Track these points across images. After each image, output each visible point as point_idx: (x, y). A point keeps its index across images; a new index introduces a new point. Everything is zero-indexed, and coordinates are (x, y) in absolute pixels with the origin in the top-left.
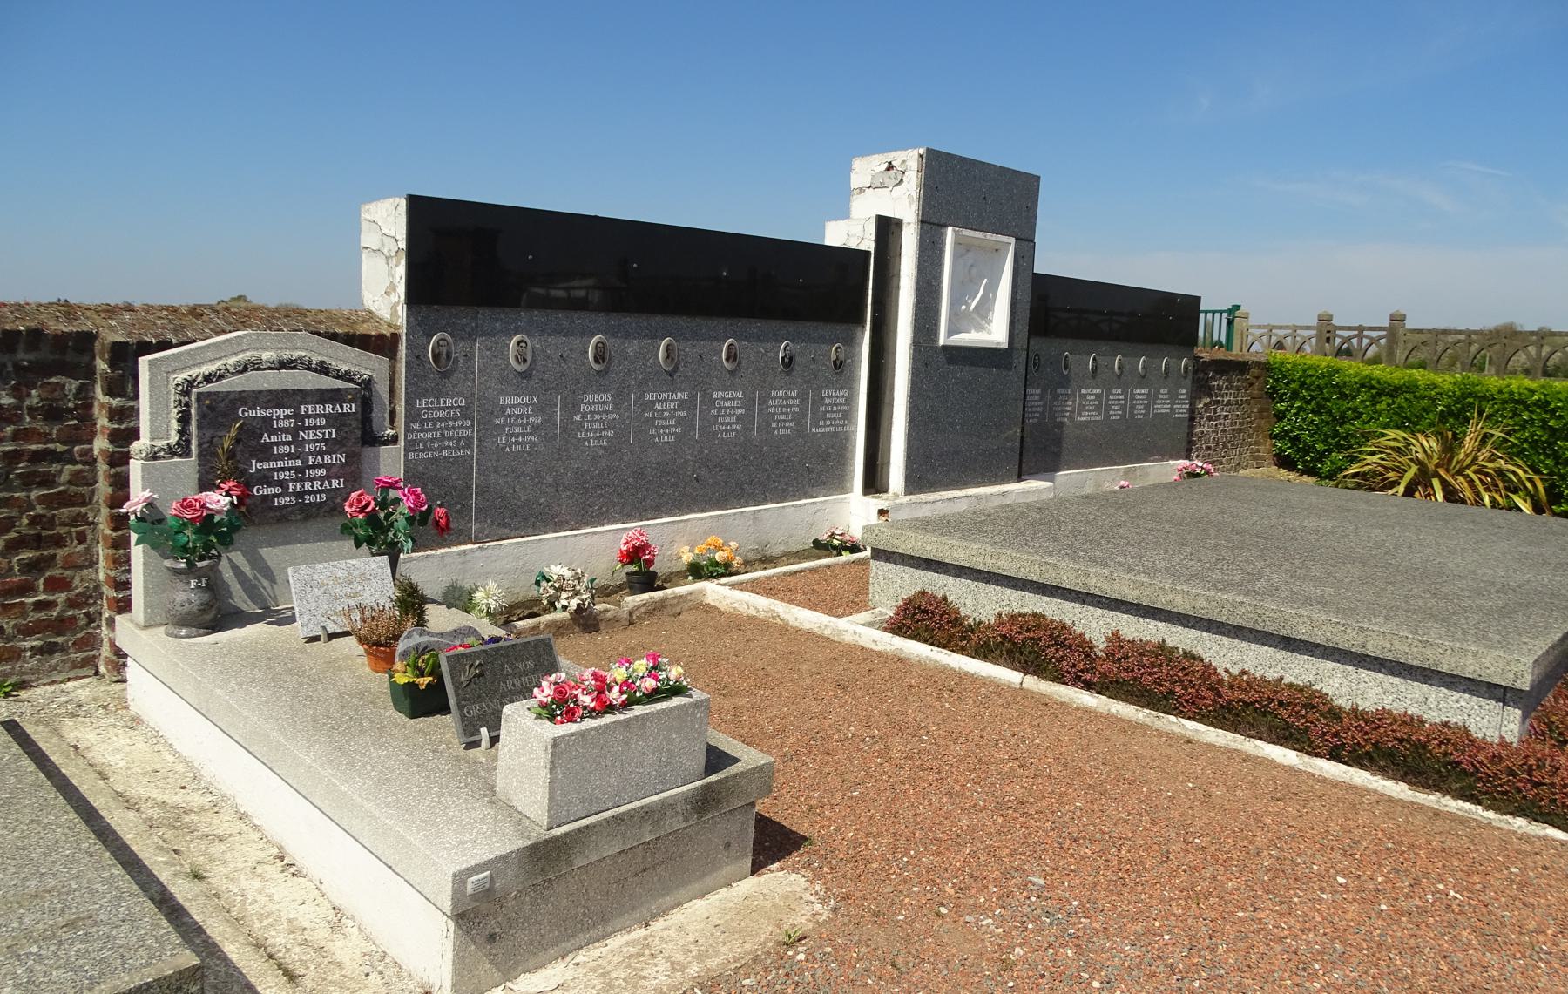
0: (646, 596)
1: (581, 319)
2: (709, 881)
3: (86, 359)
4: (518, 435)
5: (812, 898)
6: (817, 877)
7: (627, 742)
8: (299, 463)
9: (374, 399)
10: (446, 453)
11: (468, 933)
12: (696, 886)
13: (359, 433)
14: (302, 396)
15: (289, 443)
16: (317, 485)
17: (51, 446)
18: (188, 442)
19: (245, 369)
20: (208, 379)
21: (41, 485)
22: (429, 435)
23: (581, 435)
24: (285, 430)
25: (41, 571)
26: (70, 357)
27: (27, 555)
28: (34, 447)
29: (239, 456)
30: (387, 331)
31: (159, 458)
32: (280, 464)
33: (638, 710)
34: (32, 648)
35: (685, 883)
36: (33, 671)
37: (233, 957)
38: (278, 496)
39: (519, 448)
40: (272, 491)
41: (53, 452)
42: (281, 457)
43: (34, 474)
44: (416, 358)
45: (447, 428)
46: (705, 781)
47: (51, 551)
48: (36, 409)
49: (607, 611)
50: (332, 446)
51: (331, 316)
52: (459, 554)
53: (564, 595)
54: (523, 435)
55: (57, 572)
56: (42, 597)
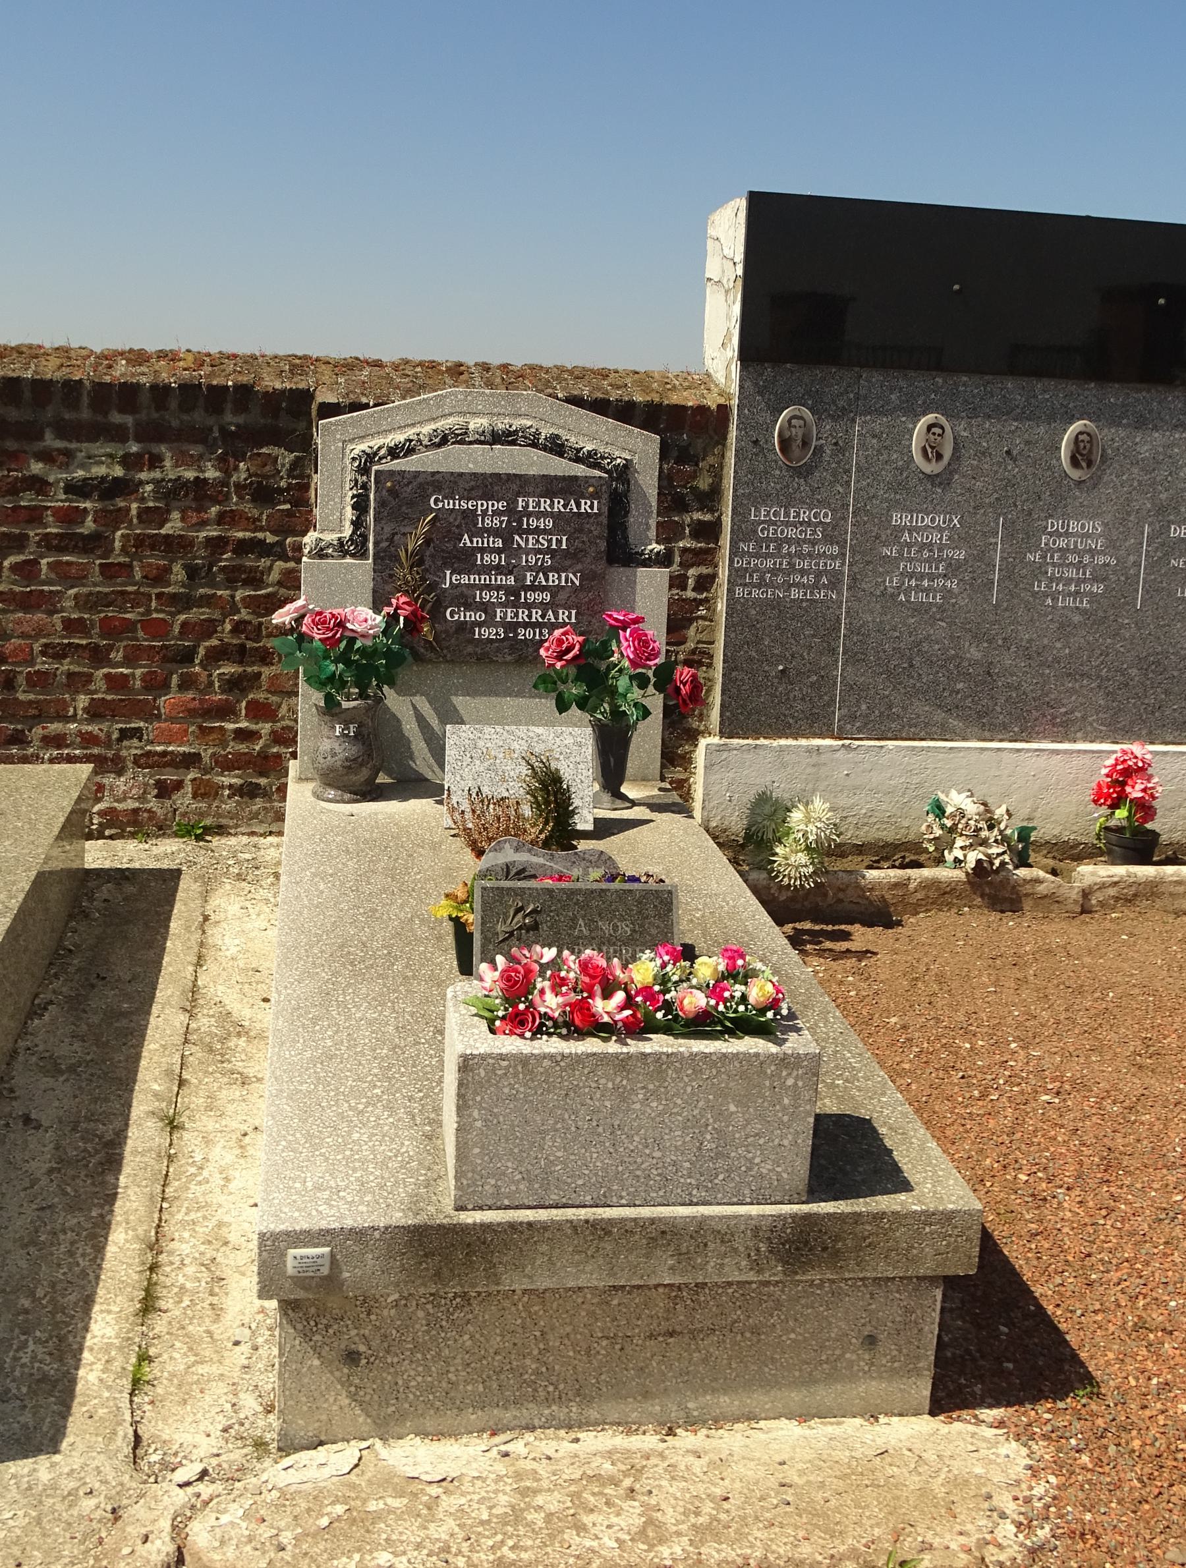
0: (1121, 870)
1: (1047, 392)
2: (825, 1394)
3: (303, 424)
4: (922, 577)
5: (1010, 1507)
6: (1058, 1466)
7: (624, 1096)
8: (511, 581)
9: (633, 496)
10: (795, 594)
11: (307, 1336)
12: (796, 1397)
13: (603, 545)
14: (519, 484)
15: (499, 551)
16: (536, 615)
17: (260, 535)
18: (365, 538)
19: (444, 441)
20: (394, 452)
21: (247, 583)
22: (769, 564)
23: (1041, 587)
24: (496, 532)
25: (244, 691)
26: (284, 422)
27: (229, 669)
28: (240, 535)
29: (427, 564)
30: (712, 401)
31: (327, 556)
32: (484, 579)
33: (659, 1043)
34: (231, 786)
35: (768, 1384)
36: (231, 815)
37: (111, 1250)
38: (480, 625)
39: (922, 597)
40: (471, 616)
41: (262, 542)
42: (486, 569)
43: (238, 569)
44: (754, 444)
45: (800, 555)
46: (806, 1208)
47: (256, 669)
48: (245, 487)
49: (1038, 881)
50: (562, 560)
51: (580, 374)
52: (809, 750)
53: (960, 842)
54: (932, 577)
55: (261, 696)
56: (243, 724)
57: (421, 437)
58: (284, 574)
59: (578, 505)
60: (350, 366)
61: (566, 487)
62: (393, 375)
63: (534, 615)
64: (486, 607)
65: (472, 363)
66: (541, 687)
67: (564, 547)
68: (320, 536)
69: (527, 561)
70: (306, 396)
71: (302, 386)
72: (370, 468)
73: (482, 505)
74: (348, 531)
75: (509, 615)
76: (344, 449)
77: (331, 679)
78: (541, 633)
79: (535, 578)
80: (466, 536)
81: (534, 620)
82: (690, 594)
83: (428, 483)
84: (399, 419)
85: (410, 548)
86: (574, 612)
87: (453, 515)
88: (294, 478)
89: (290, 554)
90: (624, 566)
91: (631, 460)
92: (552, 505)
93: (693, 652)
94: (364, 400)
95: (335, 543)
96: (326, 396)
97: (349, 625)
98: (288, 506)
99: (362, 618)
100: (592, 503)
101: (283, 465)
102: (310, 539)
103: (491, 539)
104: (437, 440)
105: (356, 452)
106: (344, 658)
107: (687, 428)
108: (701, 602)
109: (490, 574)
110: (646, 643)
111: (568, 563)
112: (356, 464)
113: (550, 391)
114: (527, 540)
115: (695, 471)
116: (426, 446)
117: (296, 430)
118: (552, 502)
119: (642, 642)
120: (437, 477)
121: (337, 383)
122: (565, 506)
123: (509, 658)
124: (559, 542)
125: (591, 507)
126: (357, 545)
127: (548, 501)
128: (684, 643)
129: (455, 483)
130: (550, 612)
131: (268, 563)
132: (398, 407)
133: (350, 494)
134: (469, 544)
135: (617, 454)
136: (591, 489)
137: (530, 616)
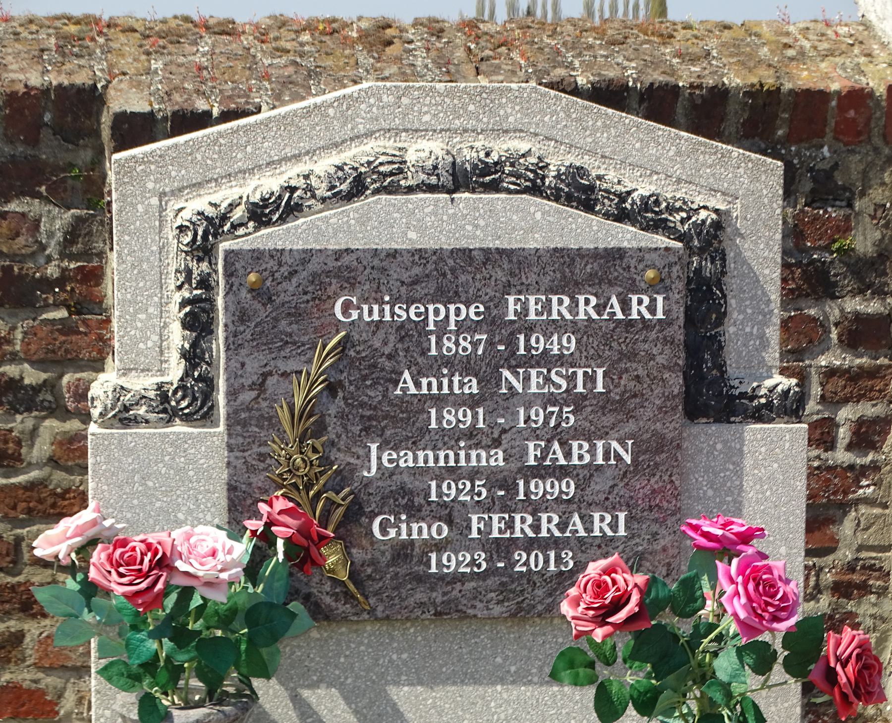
3: (86, 155)
9: (732, 283)
13: (676, 383)
14: (512, 267)
15: (473, 402)
16: (549, 524)
18: (209, 383)
19: (358, 188)
20: (260, 214)
24: (467, 366)
26: (49, 150)
29: (333, 429)
31: (135, 421)
32: (445, 457)
38: (440, 547)
40: (423, 531)
42: (449, 438)
50: (598, 413)
57: (314, 181)
58: (61, 444)
59: (626, 306)
60: (171, 35)
61: (605, 270)
62: (257, 50)
63: (544, 525)
64: (449, 513)
65: (406, 20)
66: (566, 674)
67: (600, 388)
68: (123, 382)
69: (528, 420)
70: (90, 99)
71: (81, 79)
72: (214, 246)
73: (437, 312)
74: (175, 371)
75: (496, 525)
76: (162, 209)
77: (150, 666)
78: (558, 559)
79: (546, 451)
80: (406, 375)
81: (544, 534)
82: (841, 456)
83: (328, 273)
84: (270, 148)
85: (298, 401)
86: (622, 516)
87: (381, 334)
88: (72, 257)
89: (71, 405)
90: (717, 421)
91: (728, 213)
92: (574, 307)
93: (851, 568)
94: (201, 105)
95: (152, 394)
96: (126, 99)
97: (180, 565)
98: (62, 313)
99: (203, 549)
100: (653, 301)
101: (51, 235)
102: (102, 386)
103: (456, 379)
104: (344, 187)
105: (186, 214)
106: (177, 632)
107: (829, 135)
108: (863, 471)
109: (456, 448)
110: (770, 588)
111: (608, 420)
112: (187, 239)
113: (560, 72)
114: (527, 379)
115: (847, 218)
116: (324, 200)
117: (71, 166)
118: (575, 303)
119: (762, 585)
120: (346, 260)
121: (148, 71)
122: (600, 309)
123: (497, 610)
124: (590, 379)
125: (652, 309)
126: (195, 399)
127: (567, 301)
128: (831, 550)
129: (384, 270)
130: (576, 518)
131: (30, 423)
132: (266, 123)
133: (177, 297)
134: (413, 390)
135: (699, 201)
136: (650, 274)
137: (536, 528)
